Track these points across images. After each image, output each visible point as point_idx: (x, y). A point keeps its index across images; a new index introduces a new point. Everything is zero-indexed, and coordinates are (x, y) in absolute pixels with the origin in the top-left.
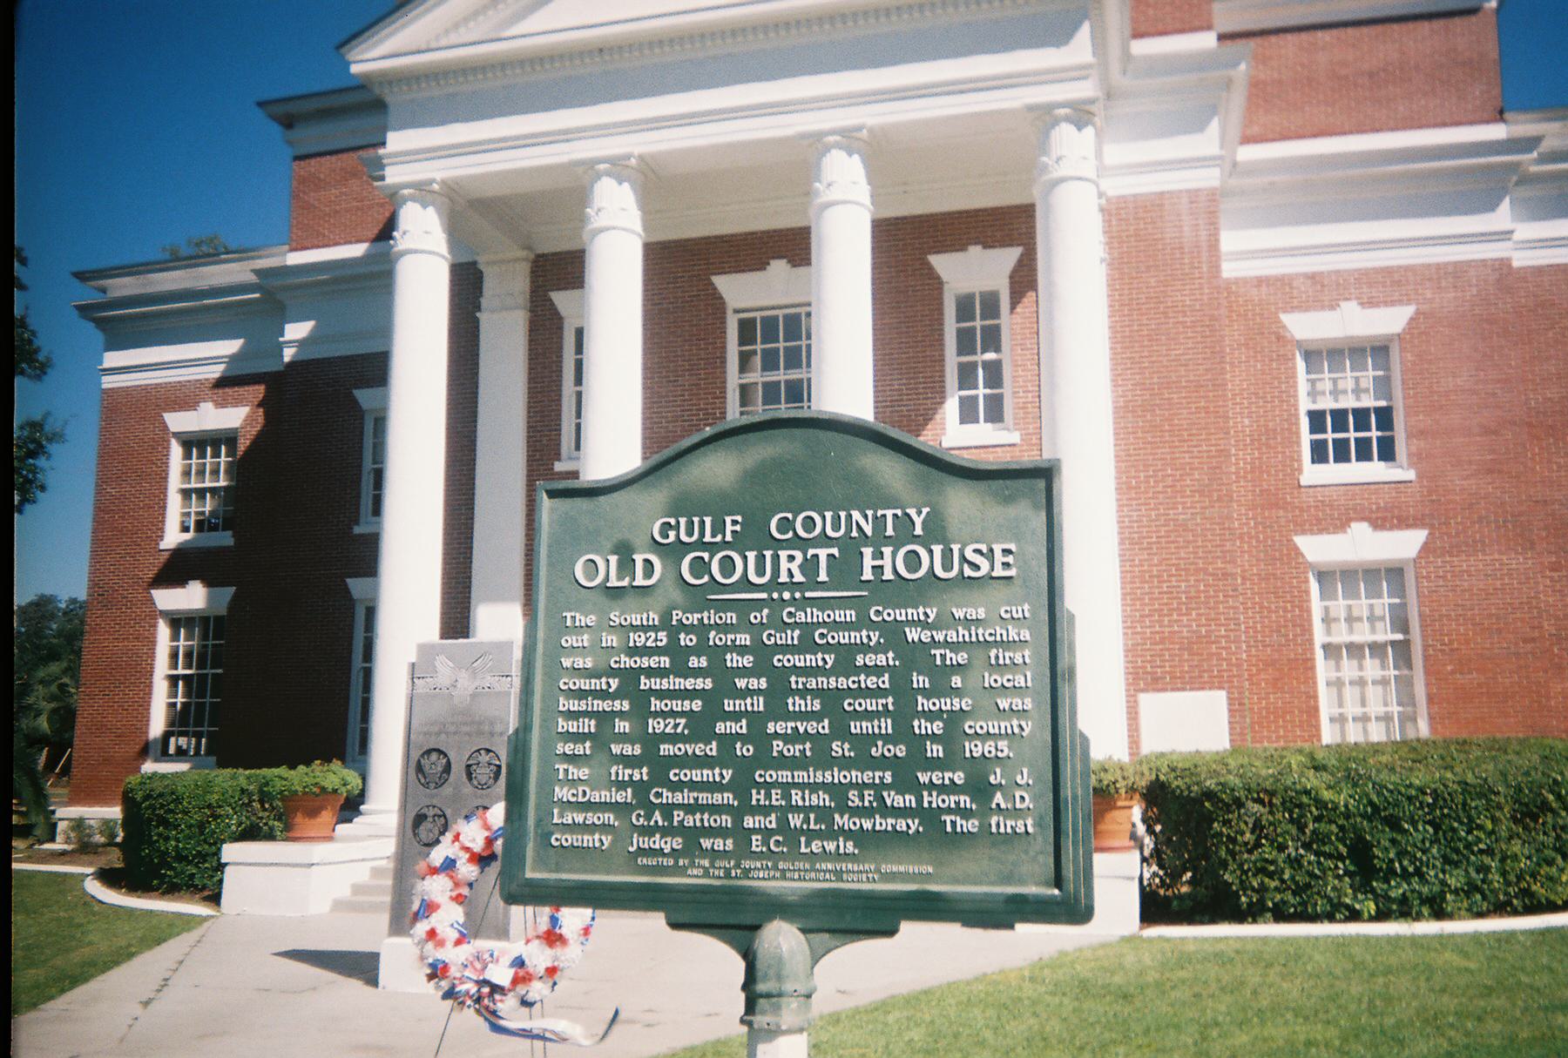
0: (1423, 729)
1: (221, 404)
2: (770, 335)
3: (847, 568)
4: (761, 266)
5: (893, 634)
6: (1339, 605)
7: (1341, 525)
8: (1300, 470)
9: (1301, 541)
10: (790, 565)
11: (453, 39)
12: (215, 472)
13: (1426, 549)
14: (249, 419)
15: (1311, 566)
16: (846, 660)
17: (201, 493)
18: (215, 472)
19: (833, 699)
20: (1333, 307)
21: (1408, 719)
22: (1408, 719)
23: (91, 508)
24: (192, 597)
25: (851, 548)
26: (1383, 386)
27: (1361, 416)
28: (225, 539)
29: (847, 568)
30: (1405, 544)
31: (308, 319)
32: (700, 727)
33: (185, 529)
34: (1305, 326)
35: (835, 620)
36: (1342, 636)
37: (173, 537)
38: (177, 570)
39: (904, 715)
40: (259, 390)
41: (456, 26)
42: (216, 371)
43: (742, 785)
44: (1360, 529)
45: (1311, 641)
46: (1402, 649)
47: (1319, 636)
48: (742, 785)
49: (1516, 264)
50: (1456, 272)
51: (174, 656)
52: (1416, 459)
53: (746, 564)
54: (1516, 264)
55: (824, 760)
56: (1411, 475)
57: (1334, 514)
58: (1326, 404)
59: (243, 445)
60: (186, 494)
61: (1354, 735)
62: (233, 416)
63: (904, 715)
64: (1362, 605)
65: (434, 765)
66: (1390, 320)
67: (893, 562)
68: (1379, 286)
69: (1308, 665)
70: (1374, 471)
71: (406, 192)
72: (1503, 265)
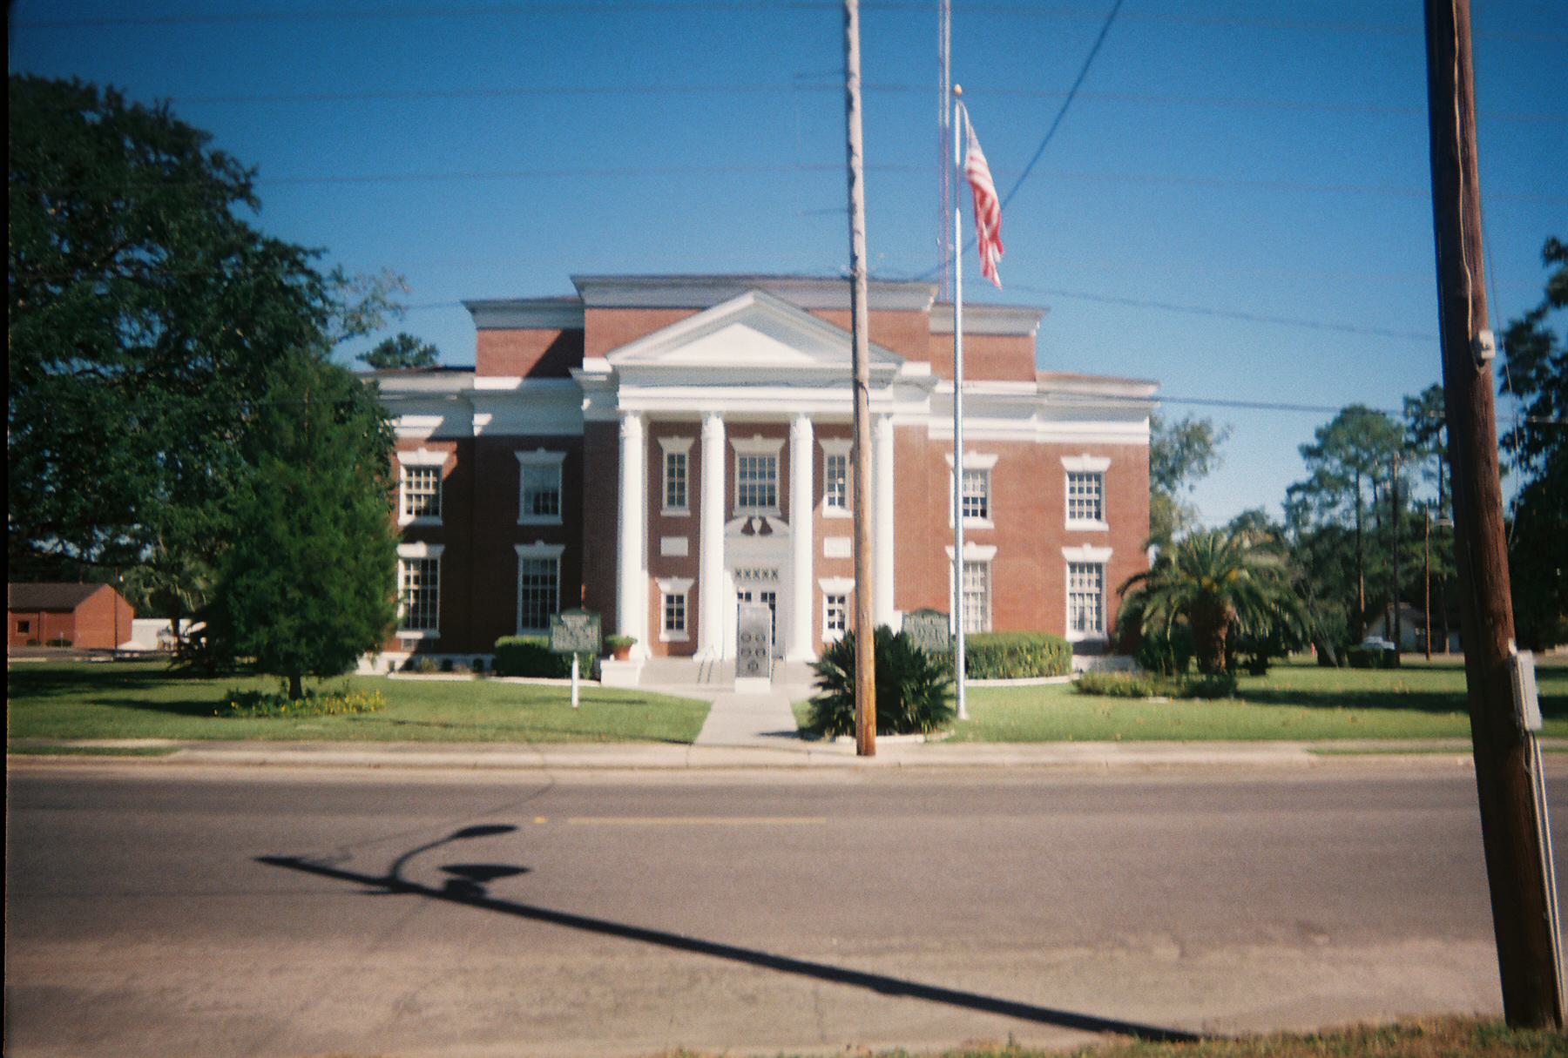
0: (989, 627)
1: (431, 450)
6: (1077, 576)
12: (427, 485)
13: (997, 556)
14: (449, 461)
17: (418, 497)
18: (427, 485)
21: (984, 621)
22: (984, 621)
24: (419, 550)
26: (984, 488)
27: (975, 500)
28: (437, 521)
30: (987, 553)
31: (437, 414)
33: (409, 512)
34: (1071, 464)
36: (1077, 589)
37: (405, 519)
38: (411, 535)
40: (454, 446)
42: (428, 433)
46: (984, 595)
47: (1068, 589)
49: (932, 435)
50: (1014, 445)
51: (408, 579)
52: (996, 520)
54: (932, 435)
58: (970, 494)
59: (445, 474)
60: (409, 496)
62: (441, 457)
64: (1086, 576)
66: (1101, 464)
68: (984, 447)
69: (1063, 603)
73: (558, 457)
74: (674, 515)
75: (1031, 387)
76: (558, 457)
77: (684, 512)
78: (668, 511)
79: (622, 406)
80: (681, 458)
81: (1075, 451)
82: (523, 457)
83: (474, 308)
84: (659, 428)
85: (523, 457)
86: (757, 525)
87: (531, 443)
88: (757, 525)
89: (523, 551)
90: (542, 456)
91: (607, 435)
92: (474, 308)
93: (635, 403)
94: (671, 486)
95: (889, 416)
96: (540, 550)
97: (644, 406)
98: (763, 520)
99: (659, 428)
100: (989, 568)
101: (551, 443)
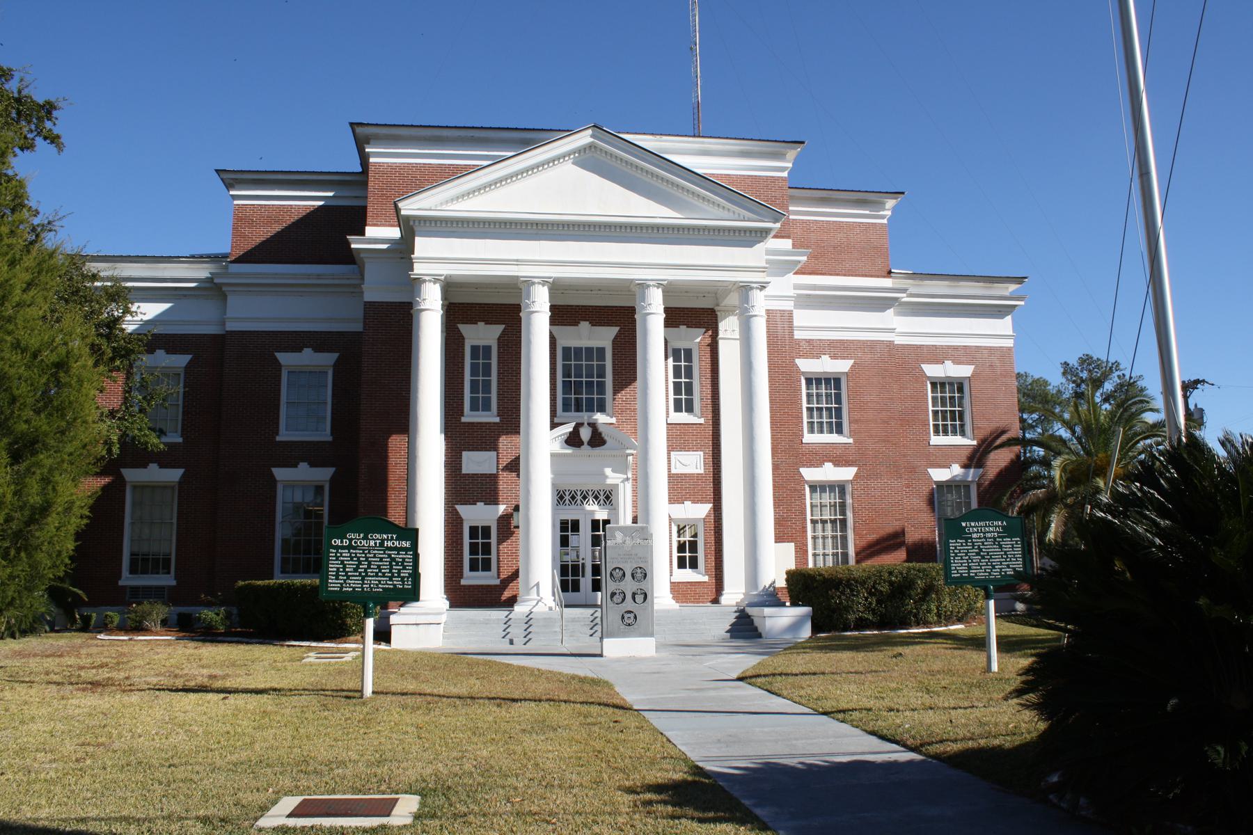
2: (578, 358)
3: (382, 544)
4: (575, 323)
5: (389, 556)
7: (820, 464)
8: (802, 436)
9: (803, 470)
10: (372, 543)
11: (444, 207)
13: (857, 476)
15: (807, 482)
16: (381, 559)
19: (379, 566)
20: (818, 357)
23: (371, 184)
25: (383, 541)
29: (382, 544)
30: (846, 474)
32: (355, 570)
34: (933, 371)
35: (380, 554)
39: (391, 569)
41: (447, 202)
43: (363, 580)
44: (828, 465)
45: (805, 519)
48: (363, 580)
50: (871, 346)
53: (364, 542)
55: (377, 576)
56: (851, 441)
57: (819, 456)
61: (820, 564)
63: (391, 569)
65: (618, 574)
67: (390, 544)
68: (838, 349)
70: (834, 438)
71: (427, 278)
72: (890, 344)
73: (327, 359)
74: (487, 416)
75: (887, 282)
76: (327, 359)
77: (491, 417)
78: (469, 416)
79: (419, 269)
80: (487, 349)
81: (937, 355)
82: (286, 359)
83: (217, 171)
84: (464, 308)
85: (286, 359)
86: (585, 434)
87: (295, 341)
88: (585, 434)
89: (280, 473)
90: (307, 358)
91: (400, 320)
92: (217, 171)
93: (437, 259)
94: (474, 385)
95: (763, 287)
96: (304, 473)
97: (445, 270)
98: (593, 425)
99: (464, 308)
100: (849, 489)
101: (320, 341)
